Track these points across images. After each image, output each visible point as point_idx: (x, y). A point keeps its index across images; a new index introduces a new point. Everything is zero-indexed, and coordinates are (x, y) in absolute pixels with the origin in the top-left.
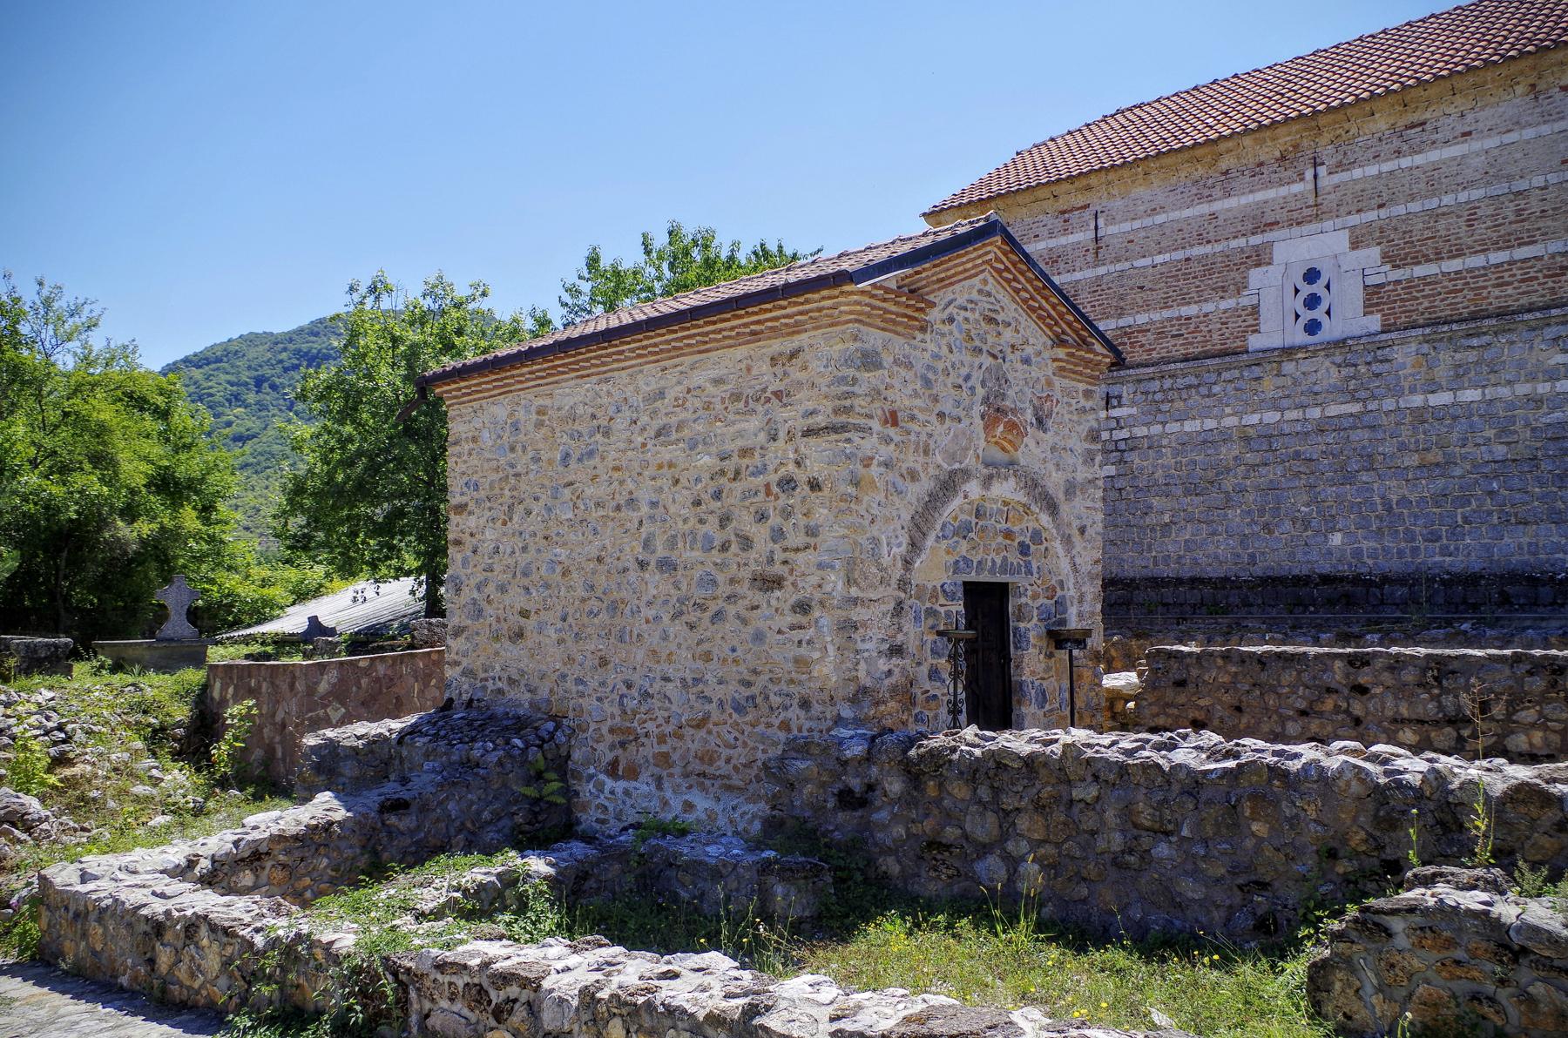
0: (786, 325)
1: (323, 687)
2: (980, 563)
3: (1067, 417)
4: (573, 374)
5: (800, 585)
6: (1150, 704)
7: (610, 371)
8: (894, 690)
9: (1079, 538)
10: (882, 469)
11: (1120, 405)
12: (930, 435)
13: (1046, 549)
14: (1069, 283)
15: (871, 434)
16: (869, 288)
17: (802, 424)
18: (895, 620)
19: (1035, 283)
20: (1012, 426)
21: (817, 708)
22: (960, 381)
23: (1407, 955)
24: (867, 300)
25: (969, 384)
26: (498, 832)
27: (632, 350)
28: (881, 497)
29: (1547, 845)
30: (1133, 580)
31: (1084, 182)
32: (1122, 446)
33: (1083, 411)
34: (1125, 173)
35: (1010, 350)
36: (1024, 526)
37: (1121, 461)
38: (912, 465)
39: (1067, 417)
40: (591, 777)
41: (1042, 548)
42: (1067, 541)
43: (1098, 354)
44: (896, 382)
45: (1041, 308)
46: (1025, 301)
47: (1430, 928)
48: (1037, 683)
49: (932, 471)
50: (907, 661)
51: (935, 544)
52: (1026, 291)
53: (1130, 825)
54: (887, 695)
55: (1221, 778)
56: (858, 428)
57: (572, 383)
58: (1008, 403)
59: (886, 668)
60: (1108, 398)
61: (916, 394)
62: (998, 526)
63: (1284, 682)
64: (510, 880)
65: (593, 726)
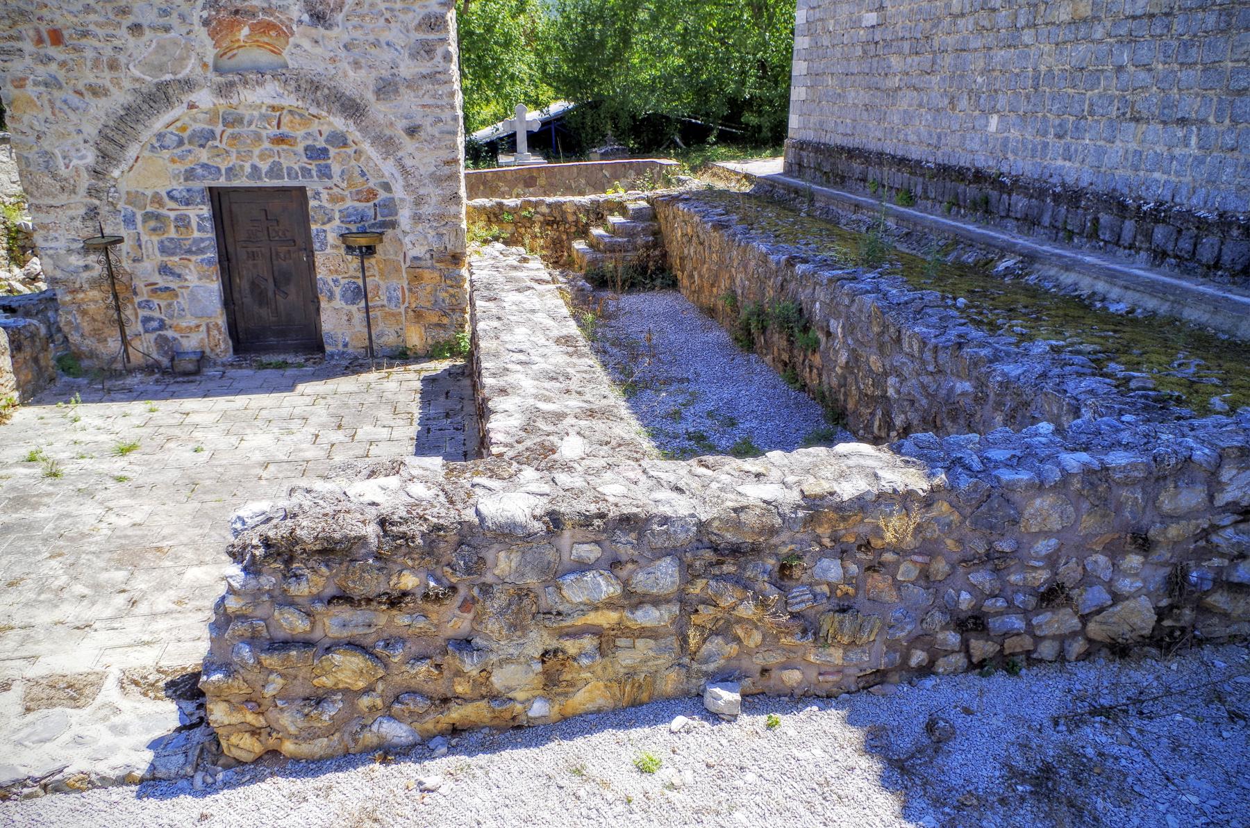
2: (229, 170)
28: (48, 113)
41: (350, 151)
42: (387, 144)
49: (127, 84)
59: (81, 263)
62: (264, 133)
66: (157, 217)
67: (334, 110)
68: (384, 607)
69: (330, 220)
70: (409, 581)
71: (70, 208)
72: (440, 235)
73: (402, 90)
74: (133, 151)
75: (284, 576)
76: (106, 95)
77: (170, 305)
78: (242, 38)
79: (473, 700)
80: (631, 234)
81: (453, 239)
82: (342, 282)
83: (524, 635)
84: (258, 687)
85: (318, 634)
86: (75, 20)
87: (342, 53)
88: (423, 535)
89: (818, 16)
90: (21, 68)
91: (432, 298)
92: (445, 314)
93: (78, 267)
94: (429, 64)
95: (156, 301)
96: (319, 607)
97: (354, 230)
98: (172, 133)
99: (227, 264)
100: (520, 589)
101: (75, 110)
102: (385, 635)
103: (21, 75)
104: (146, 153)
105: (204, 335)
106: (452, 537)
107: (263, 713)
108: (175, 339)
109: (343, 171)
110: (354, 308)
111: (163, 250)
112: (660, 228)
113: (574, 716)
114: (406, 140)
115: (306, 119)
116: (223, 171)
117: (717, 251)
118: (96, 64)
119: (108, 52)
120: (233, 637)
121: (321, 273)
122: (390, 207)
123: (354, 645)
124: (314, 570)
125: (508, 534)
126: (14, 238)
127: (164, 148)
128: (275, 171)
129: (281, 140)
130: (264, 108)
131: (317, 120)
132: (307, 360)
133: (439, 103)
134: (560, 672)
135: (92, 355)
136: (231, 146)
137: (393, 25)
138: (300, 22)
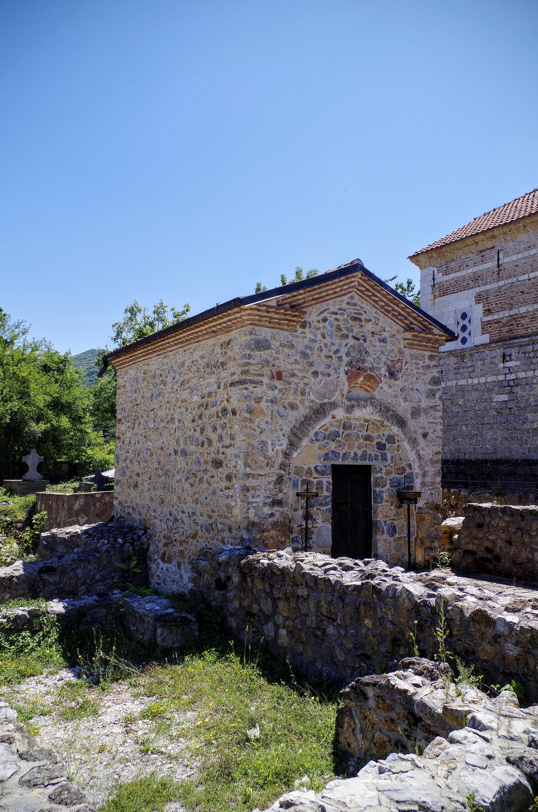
0: (225, 327)
1: (76, 507)
2: (344, 454)
3: (415, 371)
4: (156, 354)
5: (229, 466)
6: (465, 537)
7: (168, 352)
8: (275, 525)
9: (423, 440)
10: (269, 404)
11: (511, 360)
12: (306, 384)
13: (398, 446)
14: (484, 291)
15: (262, 385)
16: (255, 307)
17: (230, 380)
18: (277, 486)
19: (388, 297)
20: (370, 378)
21: (234, 532)
22: (331, 354)
23: (372, 712)
24: (257, 313)
25: (338, 355)
26: (104, 585)
27: (173, 341)
28: (269, 419)
29: (489, 651)
30: (517, 461)
31: (491, 234)
32: (512, 383)
33: (428, 367)
34: (513, 227)
35: (370, 335)
36: (381, 433)
37: (511, 392)
38: (292, 401)
39: (415, 371)
40: (155, 560)
41: (396, 445)
42: (413, 442)
43: (436, 335)
44: (281, 356)
45: (393, 310)
46: (382, 307)
47: (382, 697)
48: (388, 522)
49: (307, 404)
50: (285, 509)
51: (310, 444)
52: (383, 301)
53: (319, 614)
54: (270, 527)
55: (353, 590)
56: (252, 382)
57: (156, 358)
58: (367, 365)
59: (269, 512)
60: (504, 356)
61: (296, 362)
62: (360, 434)
63: (534, 529)
64: (34, 615)
65: (158, 534)
67: (394, 423)
71: (269, 477)
76: (297, 409)
78: (359, 382)
81: (437, 496)
90: (260, 392)
94: (433, 401)
98: (321, 432)
101: (282, 416)
103: (260, 396)
110: (392, 539)
116: (341, 455)
128: (364, 456)
130: (362, 420)
131: (383, 428)
137: (419, 380)
138: (385, 376)
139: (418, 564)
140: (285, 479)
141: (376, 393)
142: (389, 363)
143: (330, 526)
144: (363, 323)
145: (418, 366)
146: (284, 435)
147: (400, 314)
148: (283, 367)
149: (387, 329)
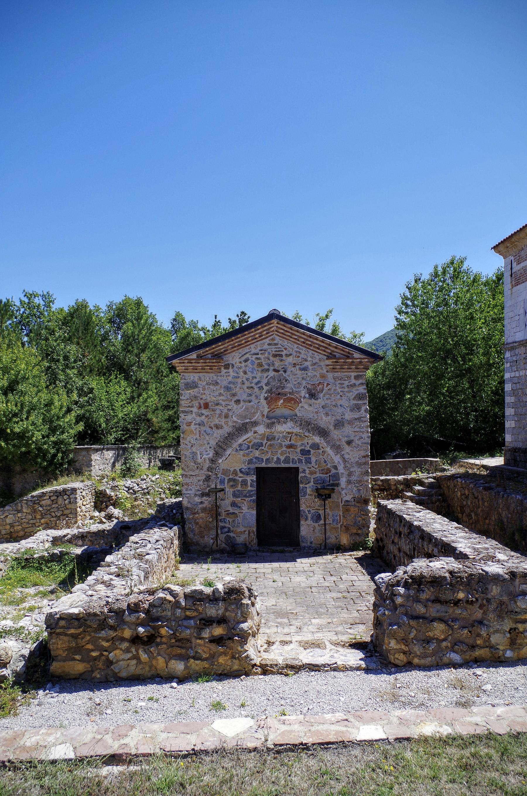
2: (267, 460)
8: (204, 510)
18: (206, 483)
22: (253, 385)
25: (259, 385)
28: (198, 436)
33: (354, 385)
41: (320, 451)
42: (337, 448)
44: (207, 392)
49: (230, 424)
59: (200, 501)
61: (220, 394)
62: (283, 443)
64: (63, 554)
66: (234, 480)
67: (315, 433)
68: (452, 605)
69: (309, 483)
70: (461, 595)
72: (359, 490)
73: (346, 425)
74: (228, 452)
75: (418, 591)
76: (221, 428)
77: (234, 521)
78: (279, 404)
79: (484, 648)
80: (430, 495)
82: (312, 512)
83: (503, 621)
84: (407, 634)
85: (427, 615)
86: (214, 399)
87: (321, 410)
88: (466, 577)
89: (518, 387)
90: (190, 418)
91: (354, 521)
92: (360, 529)
93: (198, 502)
94: (358, 414)
95: (228, 519)
96: (430, 604)
97: (320, 487)
98: (245, 444)
99: (260, 504)
100: (501, 601)
102: (451, 617)
104: (234, 453)
105: (247, 536)
106: (476, 579)
107: (407, 646)
108: (234, 537)
109: (316, 460)
110: (316, 525)
111: (235, 495)
112: (444, 492)
113: (522, 658)
114: (346, 446)
115: (301, 437)
116: (264, 460)
117: (488, 501)
118: (220, 416)
119: (225, 411)
120: (399, 613)
121: (303, 507)
122: (336, 477)
123: (441, 620)
124: (428, 589)
125: (496, 578)
126: (98, 497)
127: (241, 450)
128: (287, 460)
129: (290, 446)
130: (285, 433)
131: (307, 438)
132: (294, 549)
133: (362, 430)
134: (516, 639)
135: (197, 544)
136: (269, 449)
138: (305, 397)
139: (342, 546)
140: (212, 478)
141: (297, 411)
142: (309, 386)
143: (255, 512)
144: (284, 358)
145: (343, 386)
146: (210, 448)
147: (321, 346)
148: (209, 399)
149: (309, 359)
